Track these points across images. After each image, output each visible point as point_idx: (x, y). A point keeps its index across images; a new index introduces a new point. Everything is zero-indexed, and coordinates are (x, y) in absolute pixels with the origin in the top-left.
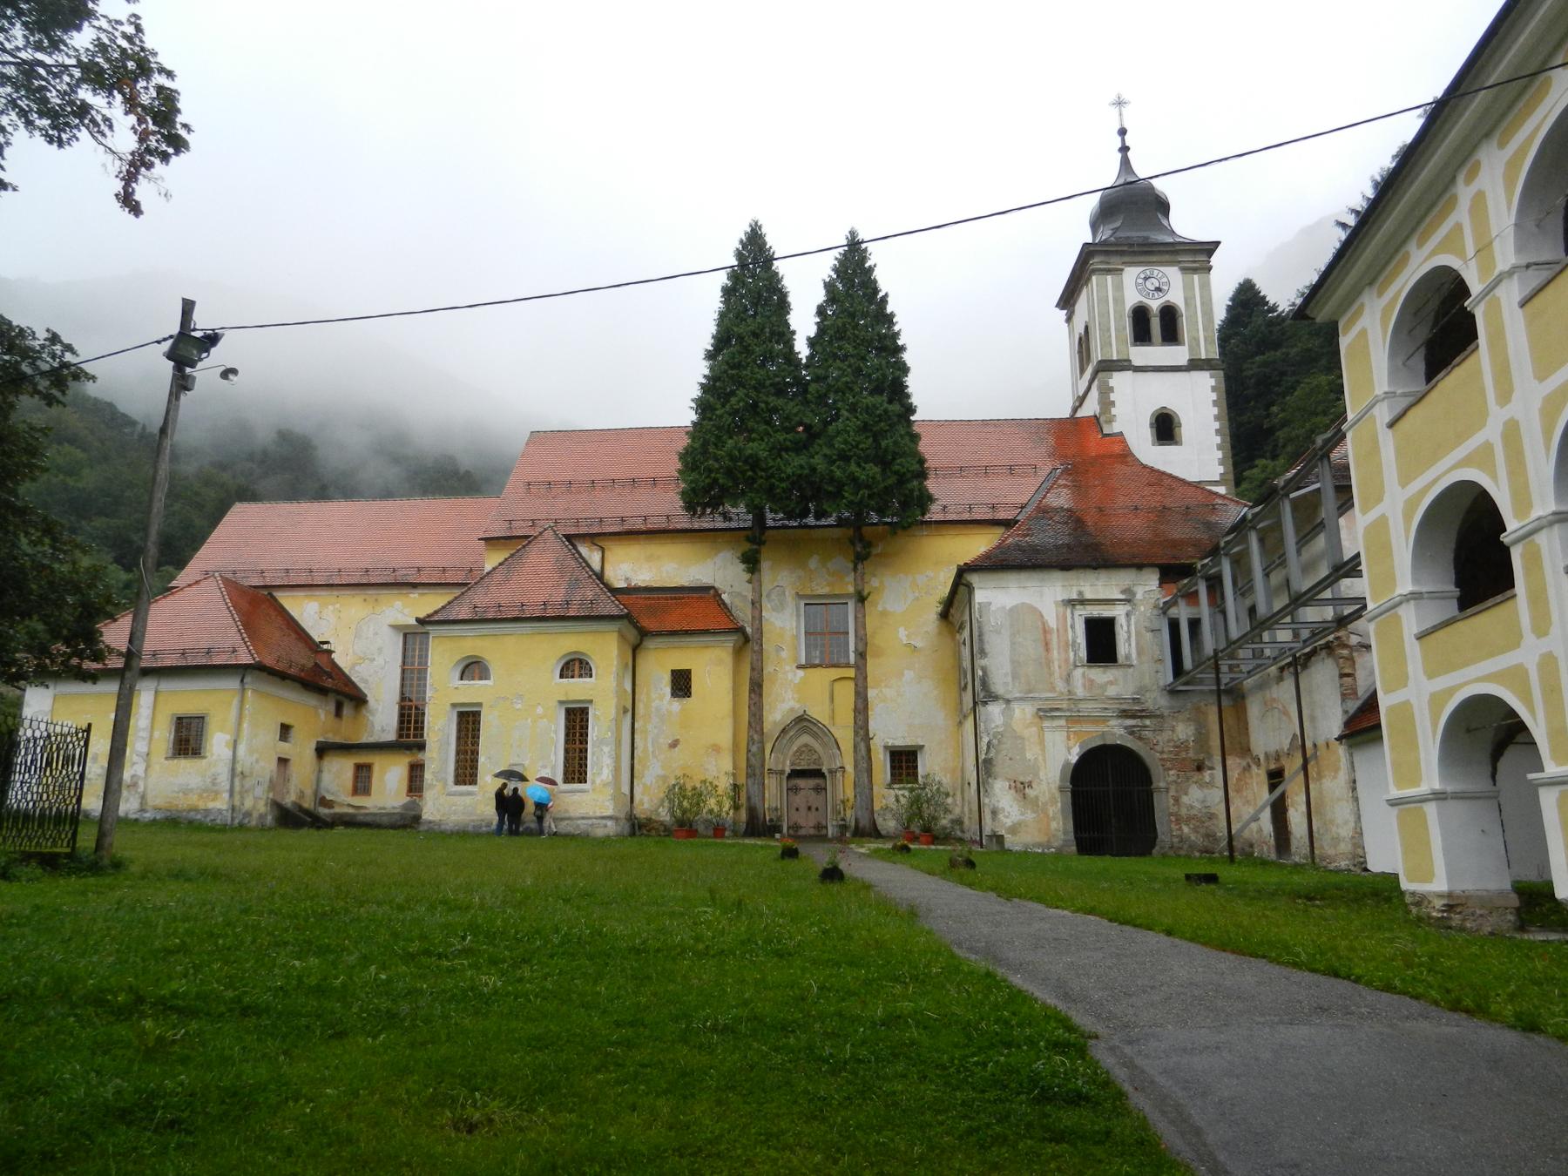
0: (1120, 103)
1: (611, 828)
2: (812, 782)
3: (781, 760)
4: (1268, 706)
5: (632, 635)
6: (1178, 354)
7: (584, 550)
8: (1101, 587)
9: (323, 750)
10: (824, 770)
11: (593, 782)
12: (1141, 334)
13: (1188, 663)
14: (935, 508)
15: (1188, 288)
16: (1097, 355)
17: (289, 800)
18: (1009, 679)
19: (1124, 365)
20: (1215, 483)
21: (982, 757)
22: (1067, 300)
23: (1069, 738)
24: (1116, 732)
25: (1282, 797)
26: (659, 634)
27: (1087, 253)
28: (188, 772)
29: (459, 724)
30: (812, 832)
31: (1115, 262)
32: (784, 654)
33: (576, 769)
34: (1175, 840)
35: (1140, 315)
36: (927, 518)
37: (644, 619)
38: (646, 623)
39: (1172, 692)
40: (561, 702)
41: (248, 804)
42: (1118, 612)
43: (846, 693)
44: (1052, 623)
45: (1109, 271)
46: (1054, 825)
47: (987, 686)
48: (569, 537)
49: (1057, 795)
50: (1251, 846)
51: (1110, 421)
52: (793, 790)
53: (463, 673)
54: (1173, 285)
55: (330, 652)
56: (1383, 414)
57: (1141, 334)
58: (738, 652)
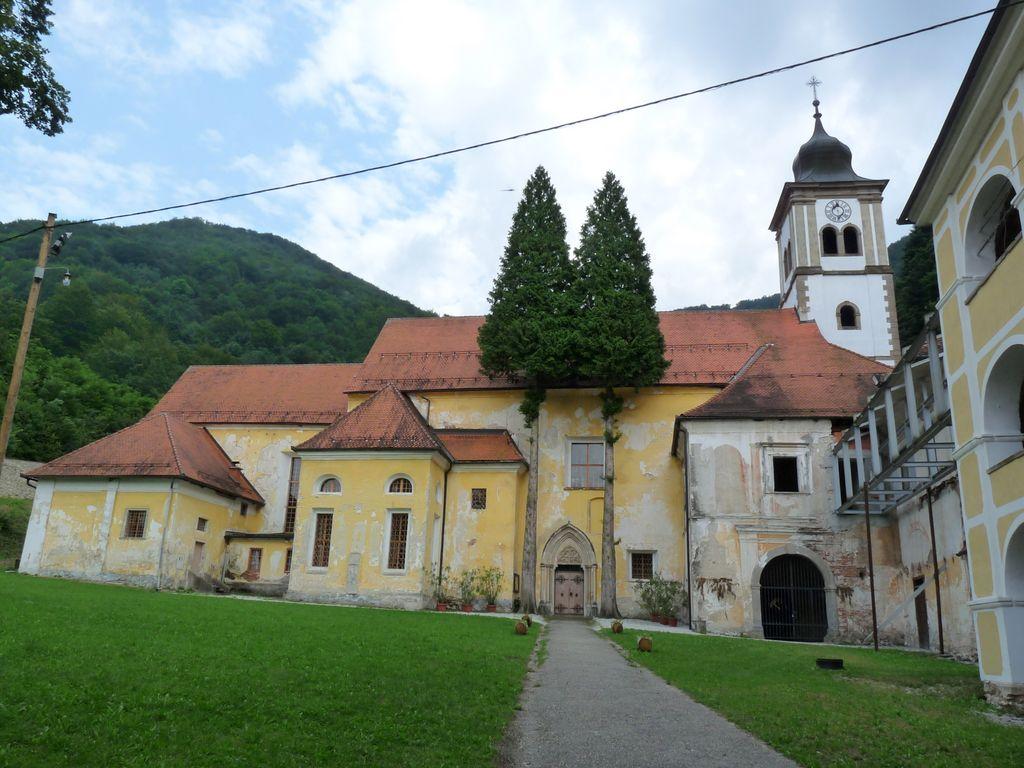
0: (814, 83)
1: (414, 605)
2: (574, 575)
3: (550, 556)
4: (914, 527)
5: (443, 463)
6: (857, 262)
7: (415, 401)
8: (786, 436)
9: (228, 539)
10: (583, 566)
11: (409, 568)
12: (830, 248)
13: (850, 493)
14: (668, 371)
15: (865, 214)
16: (797, 264)
17: (203, 571)
18: (714, 502)
19: (816, 271)
20: (887, 358)
21: (692, 560)
22: (777, 224)
23: (759, 549)
24: (796, 545)
25: (923, 593)
26: (464, 462)
27: (789, 189)
28: (134, 549)
29: (393, 522)
30: (572, 611)
31: (810, 195)
32: (555, 480)
33: (397, 559)
34: (842, 630)
35: (829, 235)
36: (662, 381)
37: (447, 451)
38: (457, 453)
39: (841, 515)
40: (389, 509)
41: (172, 573)
42: (799, 453)
43: (598, 509)
44: (748, 459)
45: (805, 202)
46: (746, 615)
47: (713, 501)
48: (405, 394)
49: (750, 592)
50: (903, 637)
51: (806, 311)
52: (561, 580)
53: (323, 486)
54: (852, 211)
55: (239, 469)
56: (962, 294)
57: (830, 248)
58: (521, 477)
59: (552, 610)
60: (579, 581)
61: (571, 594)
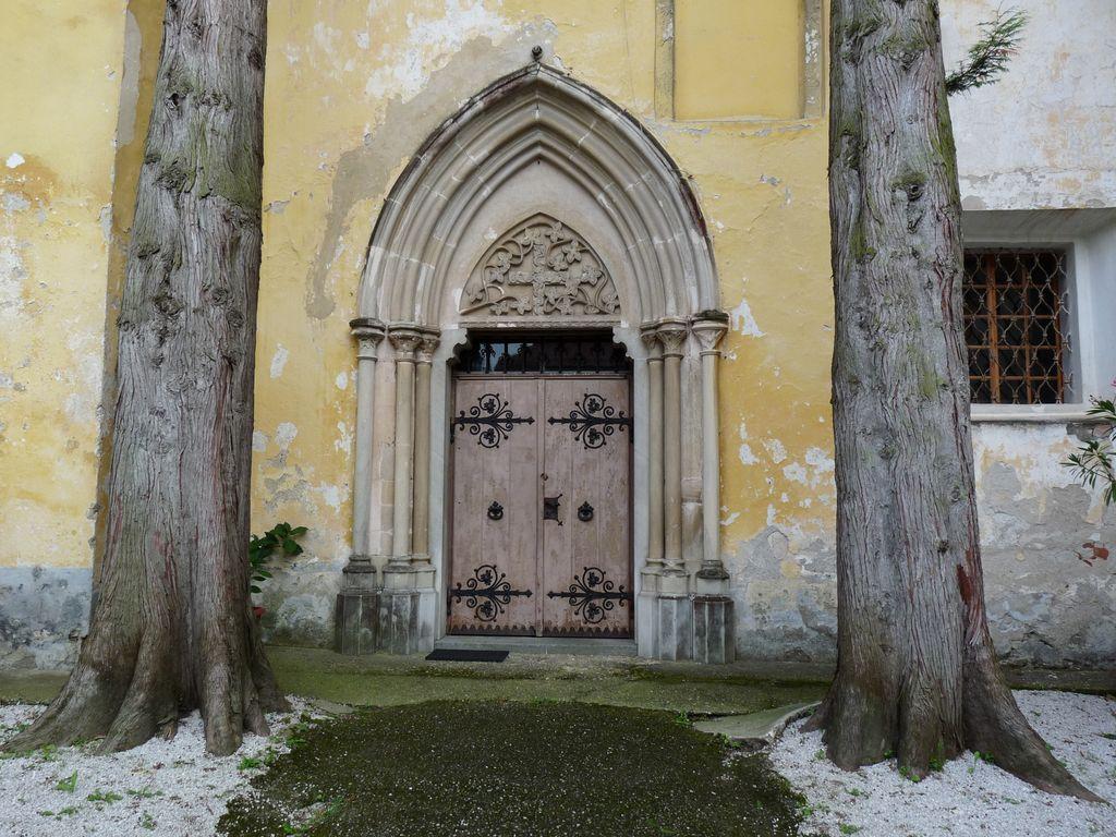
2: (565, 391)
10: (626, 332)
30: (560, 613)
52: (492, 423)
59: (430, 610)
60: (599, 424)
61: (551, 508)
